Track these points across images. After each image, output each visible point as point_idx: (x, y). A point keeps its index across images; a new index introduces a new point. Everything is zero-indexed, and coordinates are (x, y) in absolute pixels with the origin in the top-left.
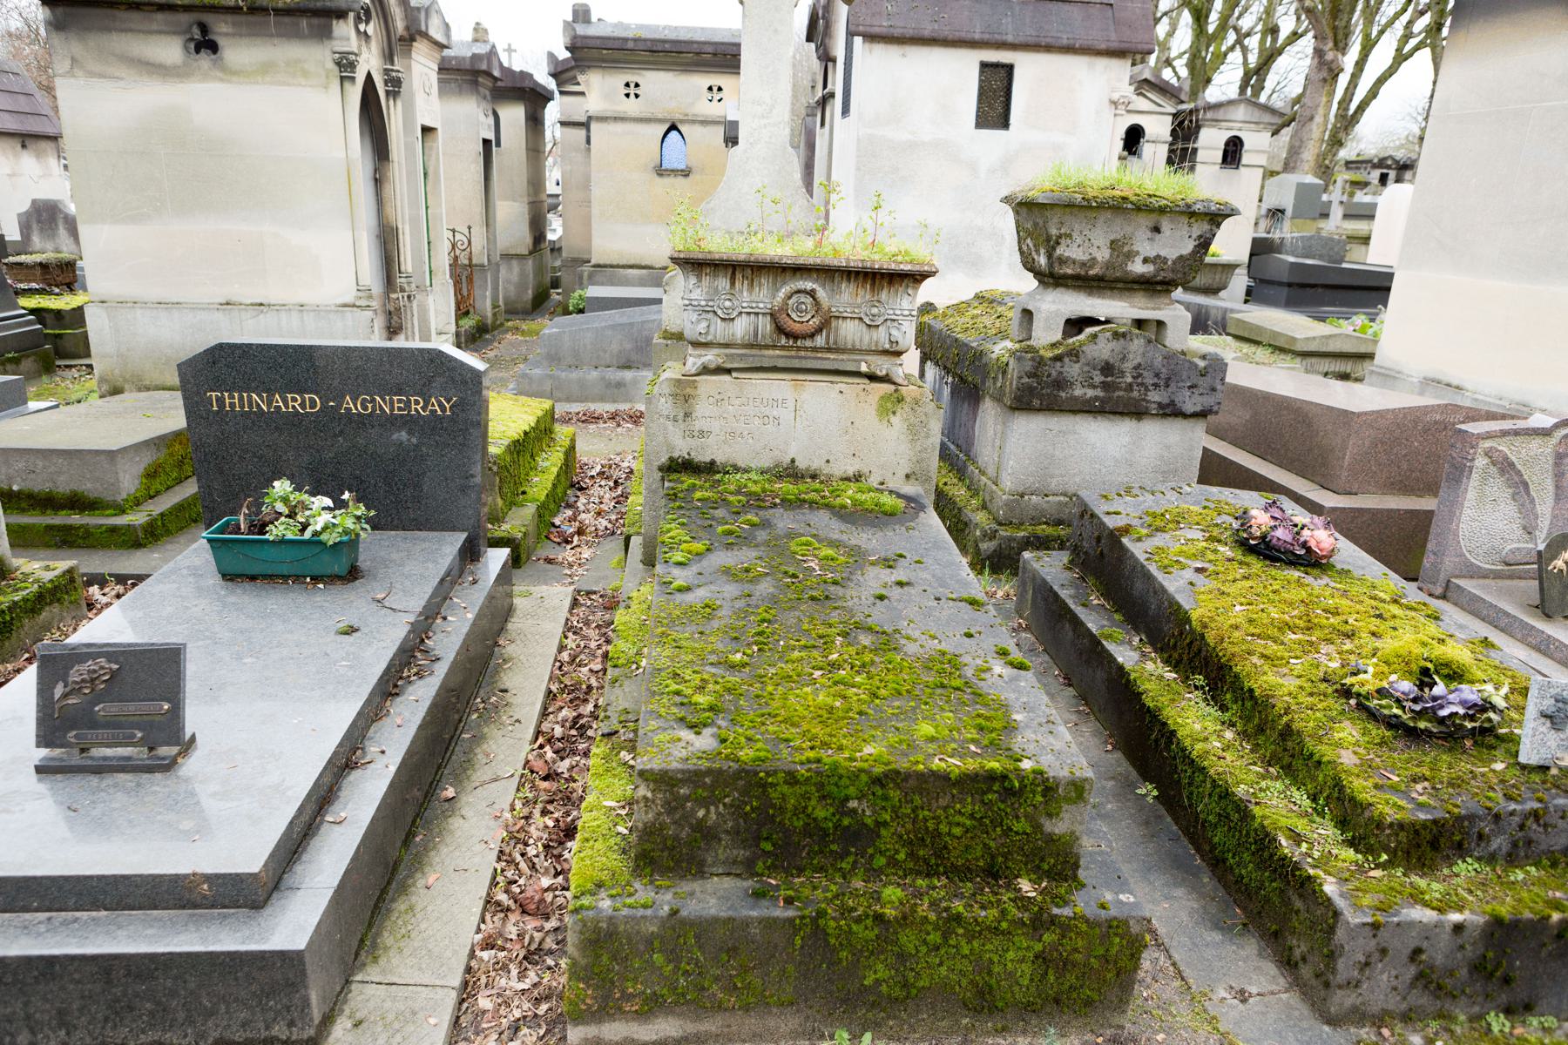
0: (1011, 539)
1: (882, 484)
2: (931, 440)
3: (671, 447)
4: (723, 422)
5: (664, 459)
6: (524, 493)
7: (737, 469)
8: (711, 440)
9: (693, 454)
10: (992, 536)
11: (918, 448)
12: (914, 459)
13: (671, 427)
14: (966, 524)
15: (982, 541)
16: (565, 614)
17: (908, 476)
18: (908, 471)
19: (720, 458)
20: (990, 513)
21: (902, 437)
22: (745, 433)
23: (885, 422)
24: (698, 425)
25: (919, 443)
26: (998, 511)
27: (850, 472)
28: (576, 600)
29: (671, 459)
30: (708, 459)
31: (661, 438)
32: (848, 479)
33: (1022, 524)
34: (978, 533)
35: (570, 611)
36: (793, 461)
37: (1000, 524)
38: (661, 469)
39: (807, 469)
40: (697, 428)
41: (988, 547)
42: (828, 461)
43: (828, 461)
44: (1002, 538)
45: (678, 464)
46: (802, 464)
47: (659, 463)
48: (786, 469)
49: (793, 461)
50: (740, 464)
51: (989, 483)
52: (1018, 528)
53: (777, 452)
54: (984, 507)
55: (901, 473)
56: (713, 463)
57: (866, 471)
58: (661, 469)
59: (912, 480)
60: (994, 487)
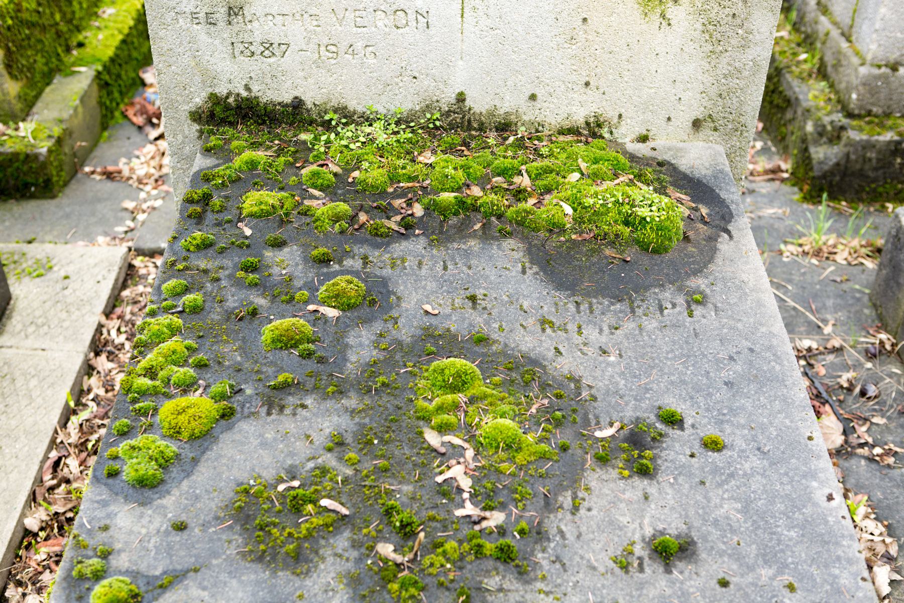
0: (868, 146)
1: (643, 139)
2: (751, 53)
3: (210, 77)
4: (310, 24)
5: (199, 100)
6: (81, 45)
7: (349, 117)
8: (289, 61)
9: (255, 88)
10: (835, 135)
11: (723, 68)
12: (713, 91)
13: (203, 37)
14: (788, 101)
15: (816, 143)
16: (96, 317)
17: (697, 124)
18: (699, 114)
19: (311, 97)
20: (832, 86)
21: (690, 48)
22: (359, 45)
23: (655, 18)
24: (259, 31)
25: (725, 59)
26: (849, 90)
27: (579, 117)
28: (131, 266)
29: (215, 99)
30: (287, 98)
31: (187, 60)
32: (573, 131)
33: (888, 115)
34: (809, 127)
35: (108, 314)
36: (461, 98)
37: (850, 115)
38: (196, 116)
39: (491, 114)
40: (258, 37)
41: (824, 154)
42: (533, 97)
43: (533, 97)
44: (850, 143)
45: (227, 108)
46: (478, 104)
47: (191, 107)
48: (448, 114)
49: (461, 98)
50: (354, 105)
51: (835, 33)
52: (882, 125)
53: (425, 83)
54: (822, 72)
55: (684, 119)
56: (298, 104)
57: (610, 114)
58: (196, 116)
59: (706, 132)
60: (844, 45)
